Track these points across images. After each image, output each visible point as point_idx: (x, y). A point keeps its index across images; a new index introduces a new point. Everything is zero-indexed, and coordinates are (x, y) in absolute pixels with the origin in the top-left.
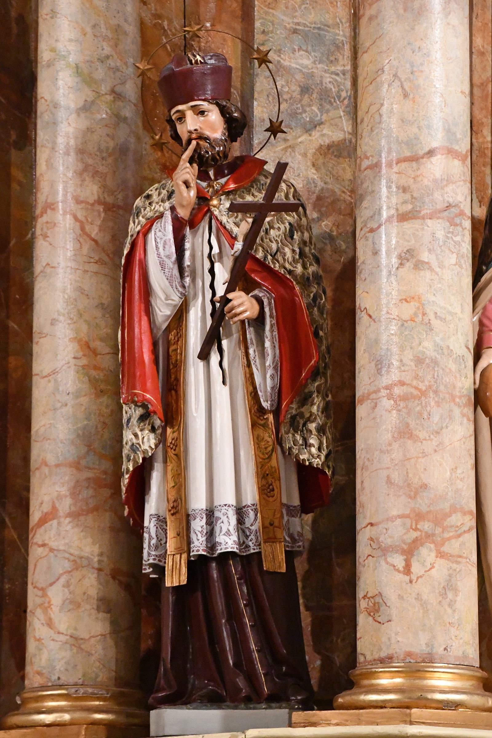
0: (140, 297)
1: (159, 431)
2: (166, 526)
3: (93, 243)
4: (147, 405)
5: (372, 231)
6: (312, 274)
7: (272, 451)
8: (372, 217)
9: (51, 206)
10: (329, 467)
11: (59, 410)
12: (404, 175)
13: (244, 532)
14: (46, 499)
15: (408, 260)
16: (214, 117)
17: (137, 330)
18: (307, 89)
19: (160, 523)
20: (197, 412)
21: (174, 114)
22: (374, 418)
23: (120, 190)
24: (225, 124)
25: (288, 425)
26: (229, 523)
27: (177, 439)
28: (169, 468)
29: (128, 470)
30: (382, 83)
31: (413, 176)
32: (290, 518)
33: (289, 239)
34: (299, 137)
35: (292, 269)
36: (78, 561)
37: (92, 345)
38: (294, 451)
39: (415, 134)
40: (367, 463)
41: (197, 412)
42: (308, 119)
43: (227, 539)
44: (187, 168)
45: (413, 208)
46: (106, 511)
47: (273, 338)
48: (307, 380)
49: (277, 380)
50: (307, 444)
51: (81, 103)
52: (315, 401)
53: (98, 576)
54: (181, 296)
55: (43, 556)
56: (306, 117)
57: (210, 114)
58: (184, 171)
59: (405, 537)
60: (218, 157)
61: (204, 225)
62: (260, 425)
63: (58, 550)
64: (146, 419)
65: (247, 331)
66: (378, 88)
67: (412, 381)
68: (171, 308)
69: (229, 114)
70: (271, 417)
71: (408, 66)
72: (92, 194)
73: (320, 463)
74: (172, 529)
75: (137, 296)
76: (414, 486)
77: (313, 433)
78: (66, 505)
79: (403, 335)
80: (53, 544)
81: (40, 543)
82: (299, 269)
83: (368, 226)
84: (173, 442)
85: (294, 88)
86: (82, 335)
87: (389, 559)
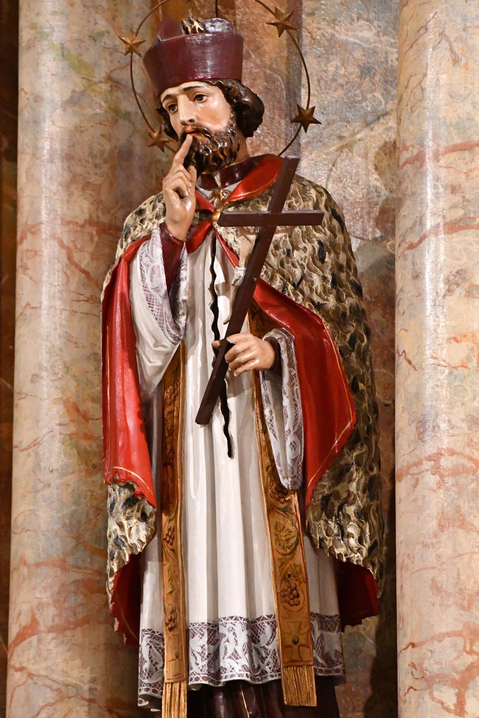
0: (123, 343)
1: (152, 520)
2: (164, 644)
3: (83, 275)
4: (132, 485)
5: (412, 246)
6: (350, 307)
7: (297, 544)
8: (411, 228)
9: (35, 229)
10: (373, 565)
11: (41, 493)
12: (452, 170)
13: (259, 653)
14: (25, 607)
15: (458, 285)
16: (216, 103)
17: (119, 387)
18: (369, 69)
19: (155, 641)
20: (196, 493)
21: (164, 101)
22: (415, 500)
23: (119, 206)
24: (232, 112)
25: (319, 509)
26: (237, 642)
27: (174, 529)
28: (166, 568)
29: (112, 570)
30: (425, 46)
31: (465, 171)
32: (326, 633)
33: (319, 263)
34: (358, 133)
35: (321, 302)
36: (64, 689)
37: (82, 408)
38: (327, 543)
39: (468, 114)
40: (407, 561)
41: (196, 493)
42: (369, 109)
43: (233, 663)
44: (180, 171)
45: (465, 214)
46: (99, 622)
47: (293, 395)
48: (342, 449)
49: (300, 449)
50: (344, 534)
51: (67, 95)
52: (354, 476)
53: (89, 709)
54: (174, 341)
55: (20, 683)
56: (367, 106)
57: (210, 99)
58: (176, 176)
59: (456, 663)
60: (221, 156)
61: (206, 247)
62: (279, 509)
63: (39, 676)
64: (134, 504)
65: (262, 386)
66: (421, 52)
67: (464, 449)
68: (162, 357)
69: (236, 98)
70: (295, 499)
71: (459, 20)
72: (83, 212)
73: (362, 559)
74: (170, 649)
75: (118, 342)
76: (468, 592)
77: (352, 519)
78: (48, 616)
79: (452, 386)
80: (32, 668)
81: (17, 666)
82: (331, 302)
83: (408, 241)
84: (170, 534)
85: (351, 69)
86: (69, 394)
87: (436, 694)
